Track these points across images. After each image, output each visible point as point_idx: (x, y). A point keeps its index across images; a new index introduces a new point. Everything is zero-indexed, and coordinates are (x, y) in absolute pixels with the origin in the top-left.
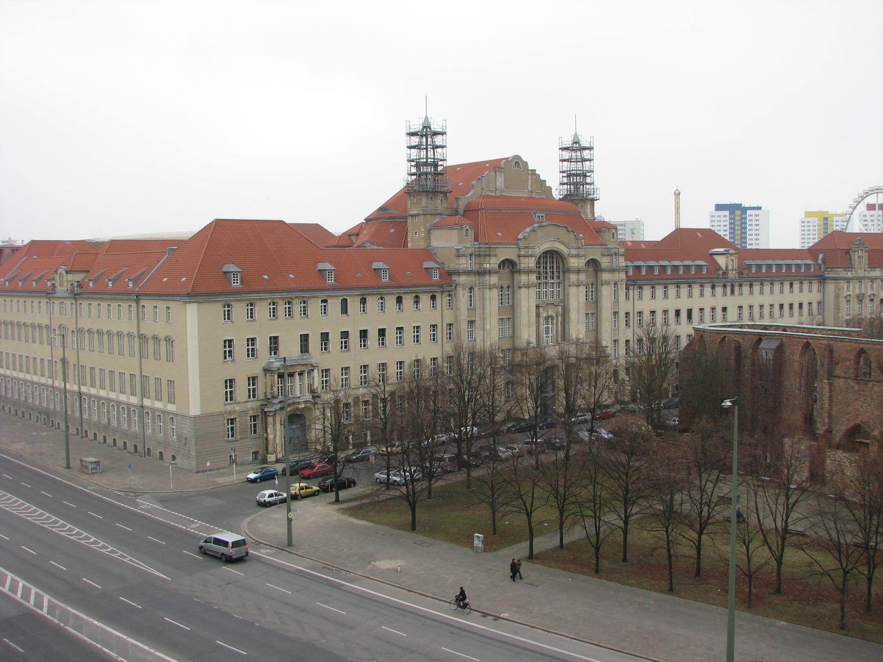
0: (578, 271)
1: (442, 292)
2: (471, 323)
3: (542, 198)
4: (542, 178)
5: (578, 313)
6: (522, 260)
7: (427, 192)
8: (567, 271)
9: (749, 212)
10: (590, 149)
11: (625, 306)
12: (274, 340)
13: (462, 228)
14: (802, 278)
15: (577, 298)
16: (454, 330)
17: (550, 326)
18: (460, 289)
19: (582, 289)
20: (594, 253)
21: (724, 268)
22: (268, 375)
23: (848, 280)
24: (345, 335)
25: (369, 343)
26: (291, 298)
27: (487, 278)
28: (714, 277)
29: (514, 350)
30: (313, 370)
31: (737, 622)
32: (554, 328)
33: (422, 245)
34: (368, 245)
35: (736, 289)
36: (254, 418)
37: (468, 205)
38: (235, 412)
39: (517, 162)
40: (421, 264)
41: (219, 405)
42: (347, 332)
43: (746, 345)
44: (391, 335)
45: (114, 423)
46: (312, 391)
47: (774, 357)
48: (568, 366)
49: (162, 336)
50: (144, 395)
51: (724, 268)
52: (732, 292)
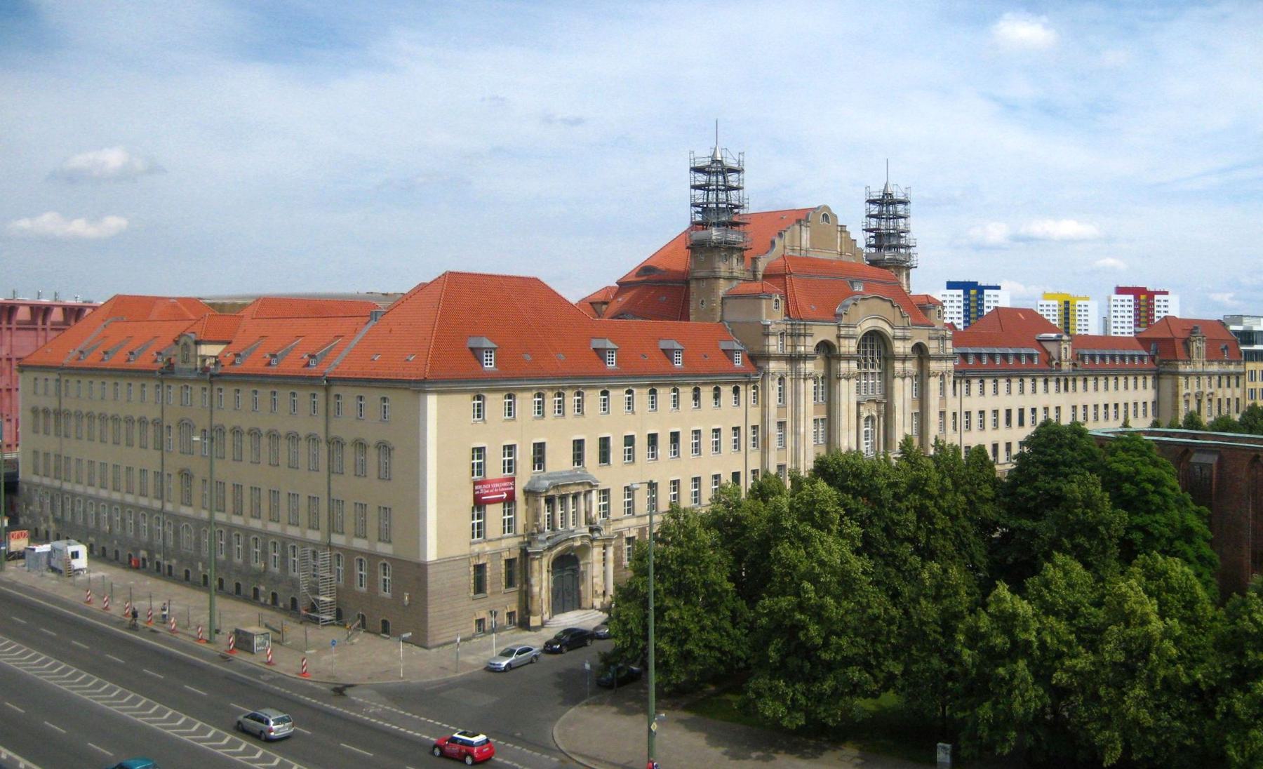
0: (904, 359)
6: (844, 342)
8: (894, 358)
9: (986, 292)
10: (904, 203)
11: (952, 405)
12: (539, 449)
14: (982, 374)
15: (903, 392)
20: (921, 336)
22: (531, 499)
23: (1187, 375)
24: (629, 440)
26: (563, 388)
30: (590, 492)
31: (437, 642)
35: (1070, 384)
36: (509, 562)
38: (484, 553)
40: (717, 346)
42: (632, 437)
44: (686, 441)
45: (118, 530)
46: (589, 521)
49: (371, 440)
50: (332, 529)
52: (1066, 389)
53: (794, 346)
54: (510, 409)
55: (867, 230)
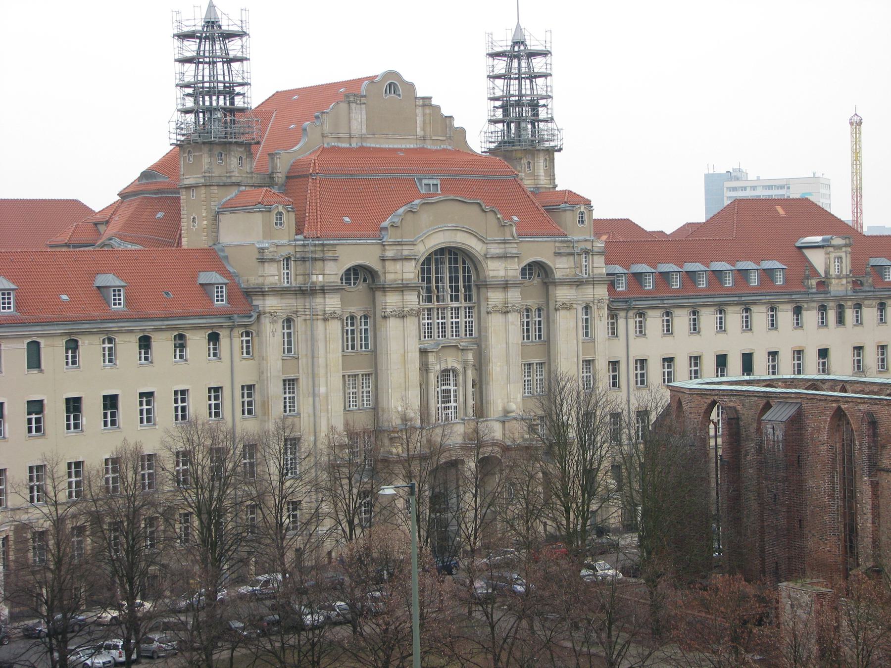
0: (505, 286)
1: (232, 328)
2: (290, 383)
3: (444, 150)
4: (445, 112)
5: (508, 362)
6: (390, 266)
7: (211, 143)
8: (484, 285)
11: (606, 349)
13: (270, 211)
14: (641, 304)
15: (504, 336)
16: (257, 397)
17: (452, 388)
18: (266, 321)
19: (515, 319)
20: (540, 250)
21: (822, 273)
24: (36, 407)
25: (84, 420)
27: (319, 300)
28: (801, 291)
29: (377, 431)
32: (463, 393)
33: (204, 242)
34: (116, 243)
35: (849, 314)
37: (294, 166)
39: (393, 84)
40: (195, 277)
42: (41, 402)
43: (747, 414)
47: (785, 435)
48: (485, 464)
51: (822, 273)
52: (841, 320)
53: (307, 275)
54: (613, 328)
55: (491, 99)
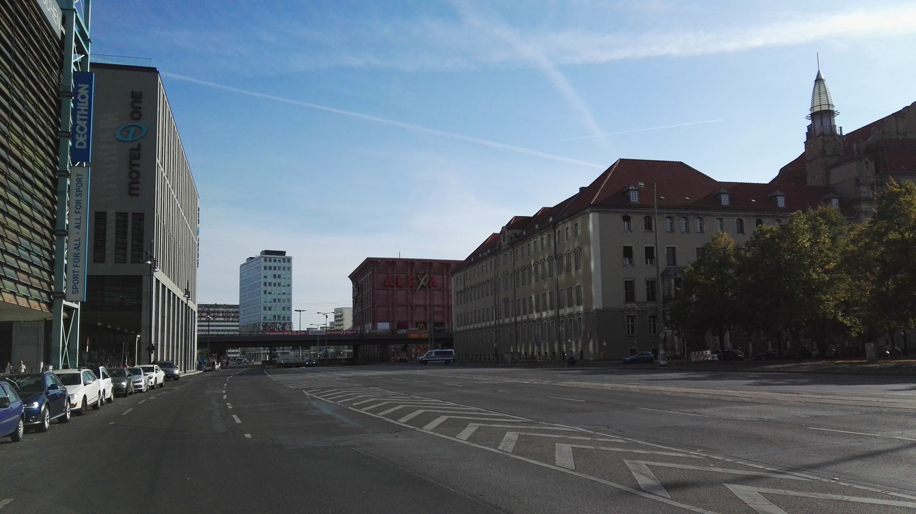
41: (619, 302)
50: (560, 306)
